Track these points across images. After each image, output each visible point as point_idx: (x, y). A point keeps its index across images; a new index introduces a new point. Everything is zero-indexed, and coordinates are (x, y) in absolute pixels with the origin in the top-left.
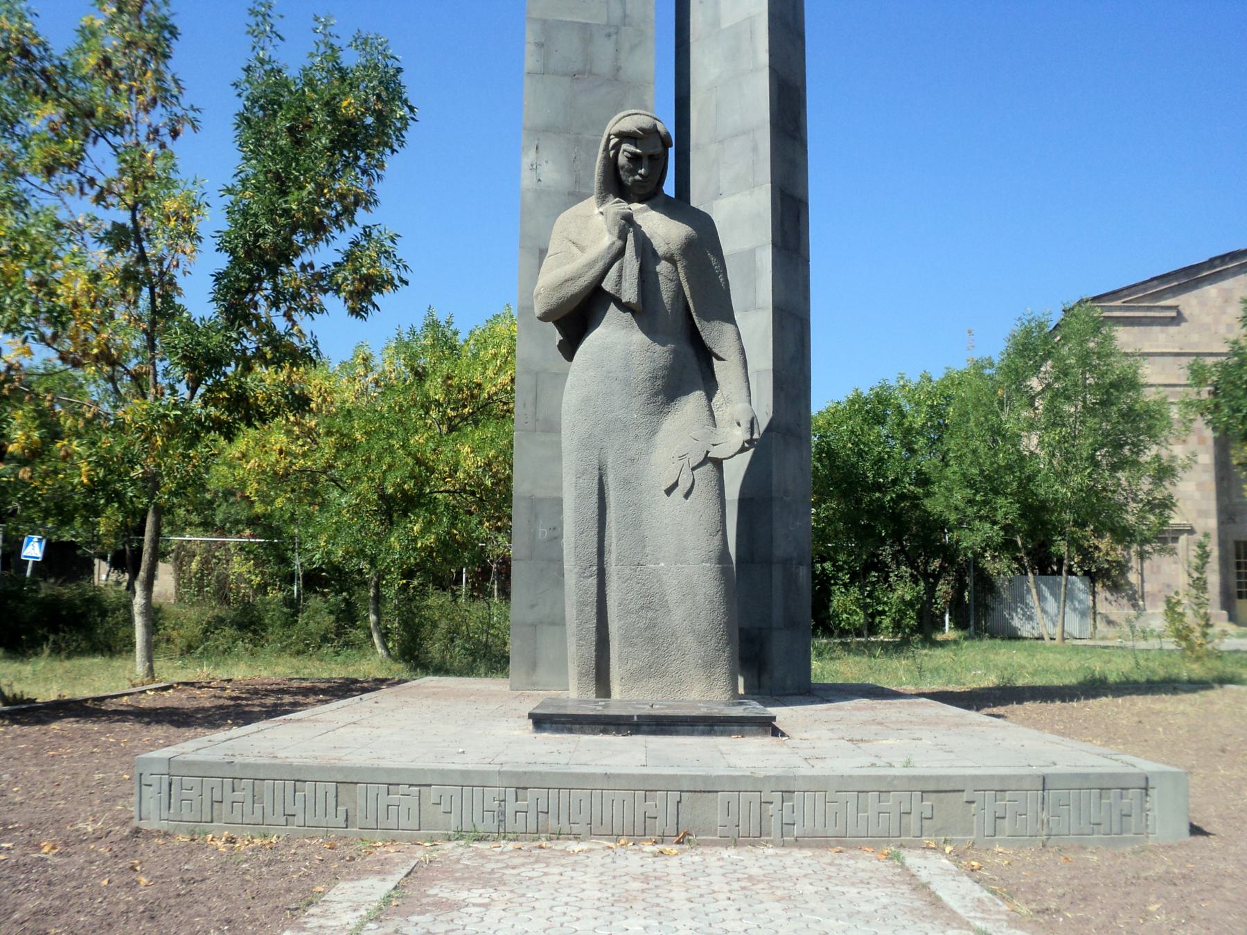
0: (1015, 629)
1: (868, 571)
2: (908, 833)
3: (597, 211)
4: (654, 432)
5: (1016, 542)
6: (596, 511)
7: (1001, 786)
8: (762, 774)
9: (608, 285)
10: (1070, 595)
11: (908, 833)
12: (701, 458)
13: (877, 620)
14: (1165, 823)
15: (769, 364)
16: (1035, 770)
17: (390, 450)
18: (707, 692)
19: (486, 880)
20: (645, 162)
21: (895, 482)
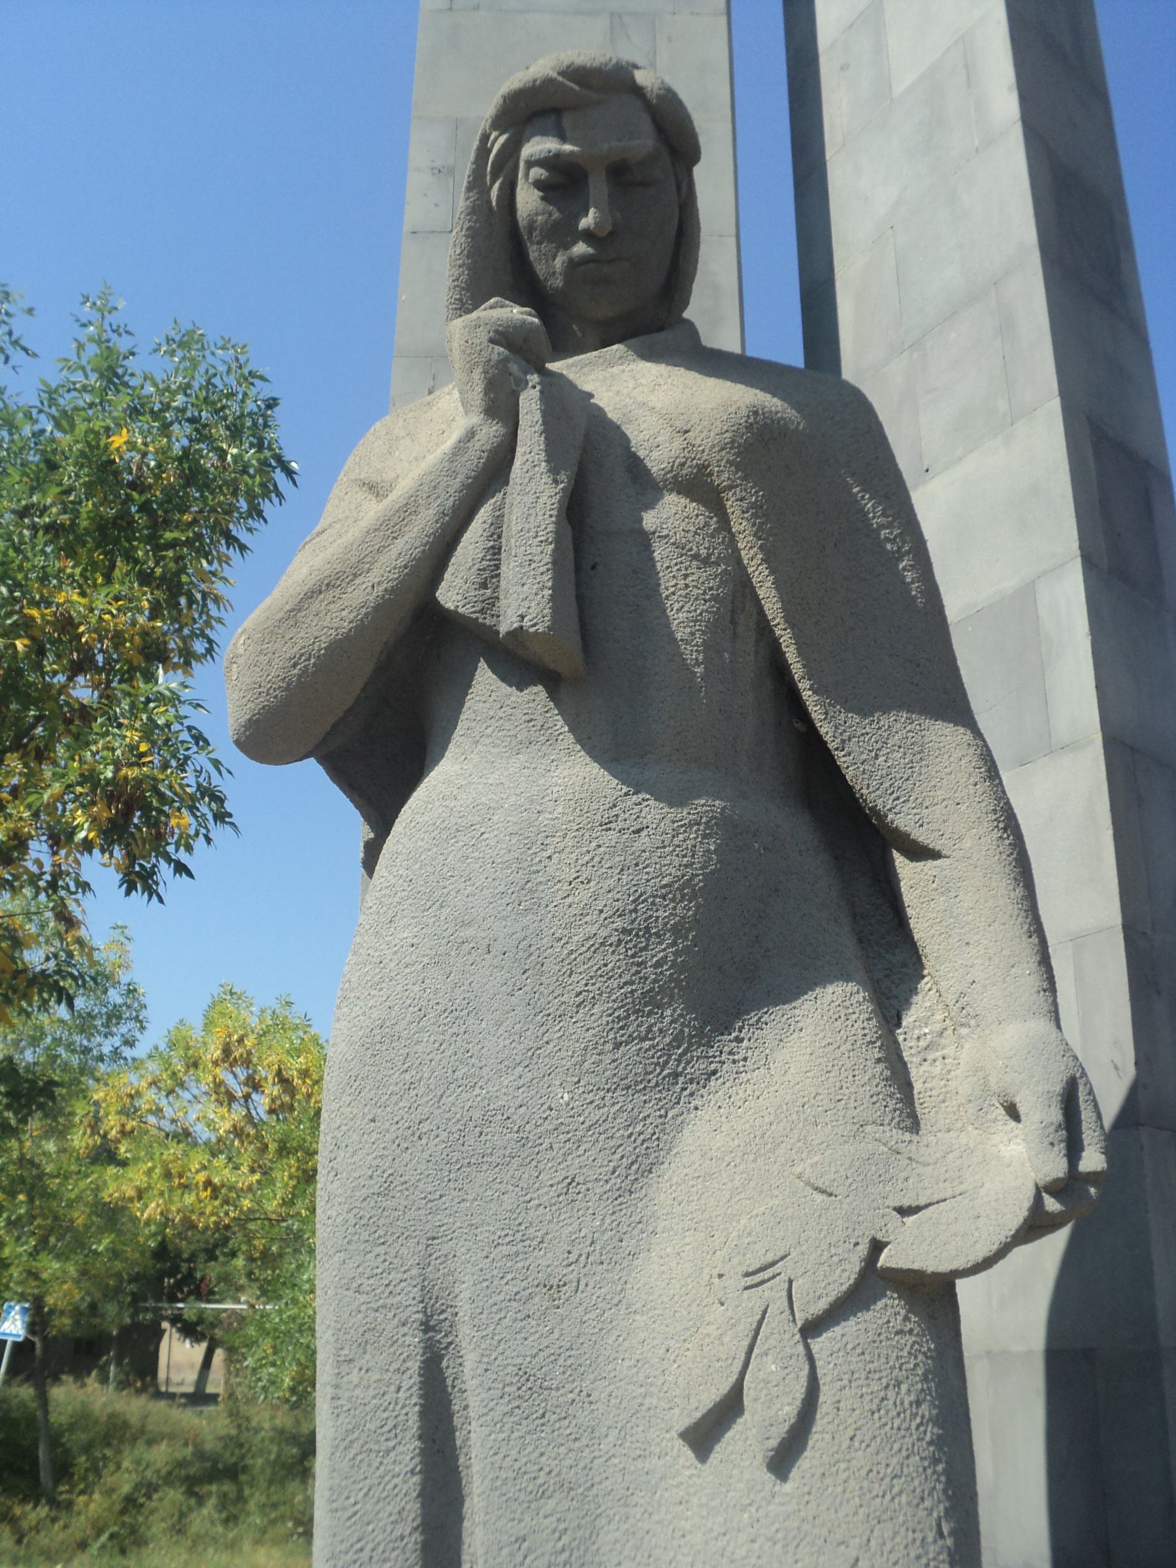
4: (642, 1163)
6: (413, 1508)
9: (454, 593)
20: (598, 186)
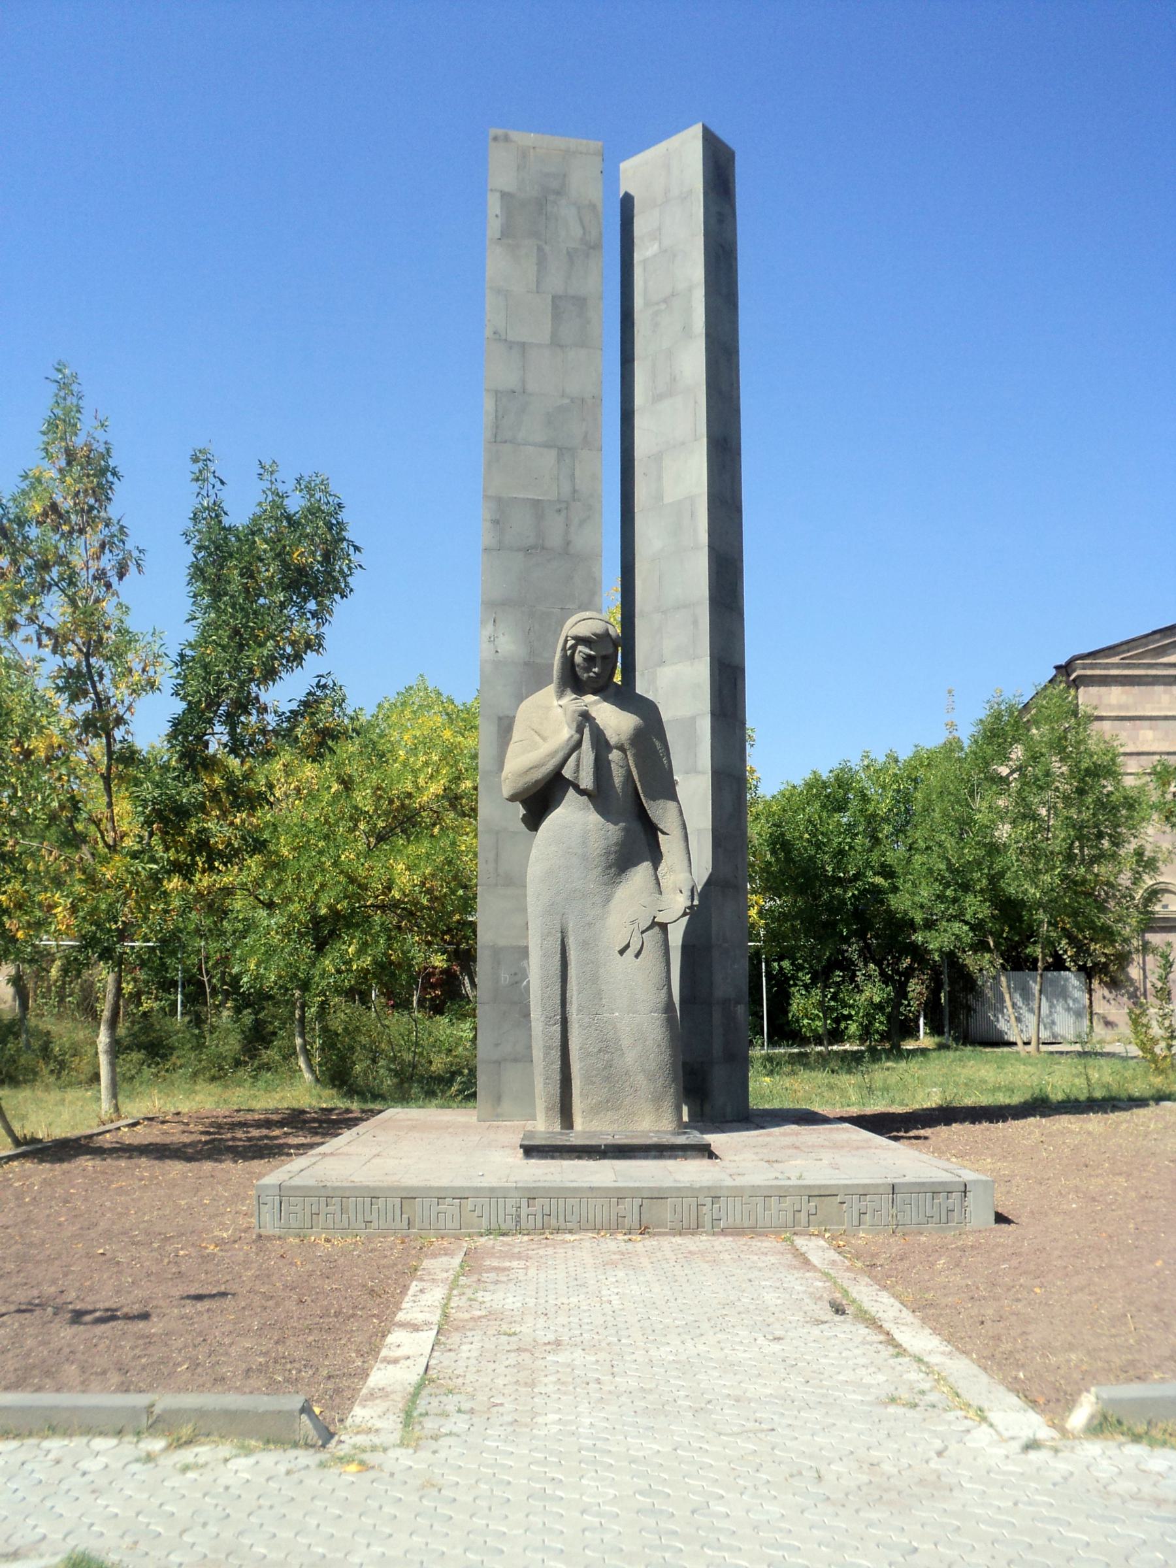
0: (1001, 1033)
1: (830, 970)
2: (799, 1224)
3: (556, 703)
4: (608, 900)
5: (988, 943)
7: (863, 1192)
8: (698, 1185)
9: (567, 772)
10: (1064, 994)
11: (799, 1224)
12: (649, 923)
13: (843, 1026)
14: (979, 1215)
15: (708, 824)
16: (890, 1181)
17: (320, 867)
18: (655, 1121)
19: (519, 1256)
20: (599, 662)
21: (857, 877)
